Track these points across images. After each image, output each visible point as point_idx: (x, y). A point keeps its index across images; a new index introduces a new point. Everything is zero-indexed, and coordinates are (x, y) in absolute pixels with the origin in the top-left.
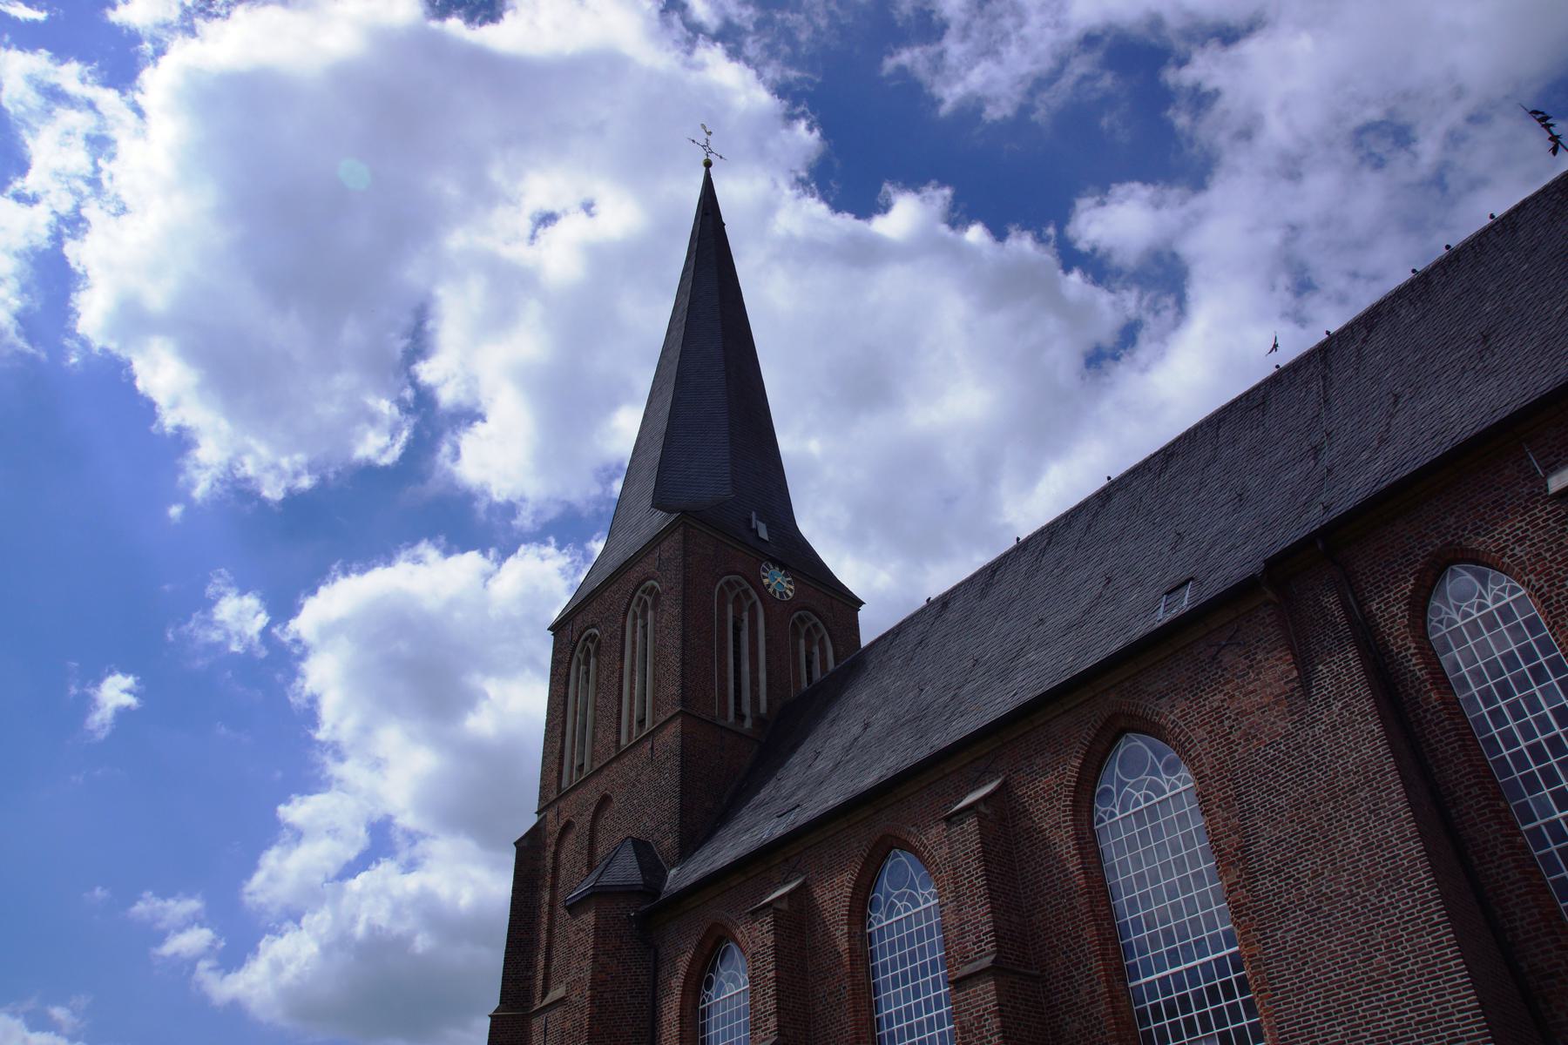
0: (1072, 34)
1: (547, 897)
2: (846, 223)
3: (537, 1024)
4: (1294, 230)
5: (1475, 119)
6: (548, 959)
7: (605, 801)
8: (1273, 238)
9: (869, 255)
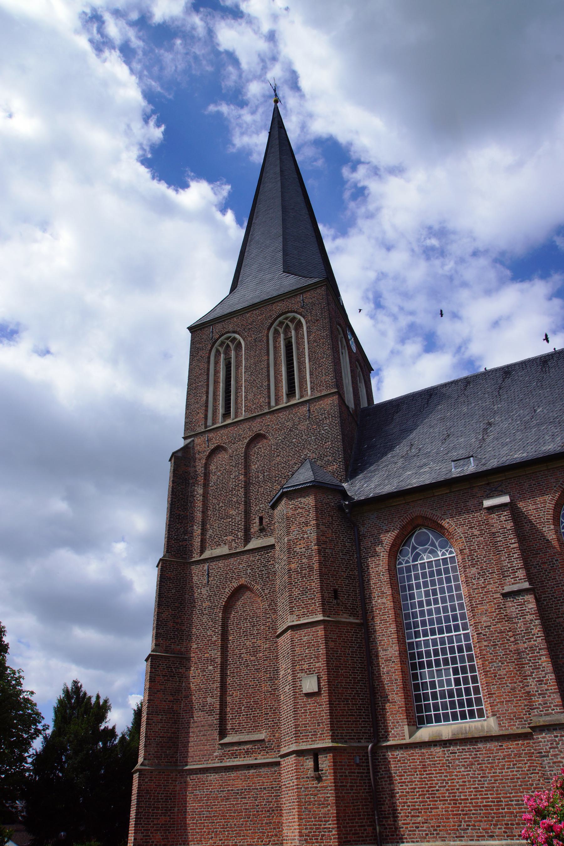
0: (310, 137)
1: (201, 491)
2: (162, 187)
3: (195, 569)
4: (382, 276)
5: (475, 254)
6: (204, 531)
7: (258, 437)
8: (372, 275)
9: (167, 209)
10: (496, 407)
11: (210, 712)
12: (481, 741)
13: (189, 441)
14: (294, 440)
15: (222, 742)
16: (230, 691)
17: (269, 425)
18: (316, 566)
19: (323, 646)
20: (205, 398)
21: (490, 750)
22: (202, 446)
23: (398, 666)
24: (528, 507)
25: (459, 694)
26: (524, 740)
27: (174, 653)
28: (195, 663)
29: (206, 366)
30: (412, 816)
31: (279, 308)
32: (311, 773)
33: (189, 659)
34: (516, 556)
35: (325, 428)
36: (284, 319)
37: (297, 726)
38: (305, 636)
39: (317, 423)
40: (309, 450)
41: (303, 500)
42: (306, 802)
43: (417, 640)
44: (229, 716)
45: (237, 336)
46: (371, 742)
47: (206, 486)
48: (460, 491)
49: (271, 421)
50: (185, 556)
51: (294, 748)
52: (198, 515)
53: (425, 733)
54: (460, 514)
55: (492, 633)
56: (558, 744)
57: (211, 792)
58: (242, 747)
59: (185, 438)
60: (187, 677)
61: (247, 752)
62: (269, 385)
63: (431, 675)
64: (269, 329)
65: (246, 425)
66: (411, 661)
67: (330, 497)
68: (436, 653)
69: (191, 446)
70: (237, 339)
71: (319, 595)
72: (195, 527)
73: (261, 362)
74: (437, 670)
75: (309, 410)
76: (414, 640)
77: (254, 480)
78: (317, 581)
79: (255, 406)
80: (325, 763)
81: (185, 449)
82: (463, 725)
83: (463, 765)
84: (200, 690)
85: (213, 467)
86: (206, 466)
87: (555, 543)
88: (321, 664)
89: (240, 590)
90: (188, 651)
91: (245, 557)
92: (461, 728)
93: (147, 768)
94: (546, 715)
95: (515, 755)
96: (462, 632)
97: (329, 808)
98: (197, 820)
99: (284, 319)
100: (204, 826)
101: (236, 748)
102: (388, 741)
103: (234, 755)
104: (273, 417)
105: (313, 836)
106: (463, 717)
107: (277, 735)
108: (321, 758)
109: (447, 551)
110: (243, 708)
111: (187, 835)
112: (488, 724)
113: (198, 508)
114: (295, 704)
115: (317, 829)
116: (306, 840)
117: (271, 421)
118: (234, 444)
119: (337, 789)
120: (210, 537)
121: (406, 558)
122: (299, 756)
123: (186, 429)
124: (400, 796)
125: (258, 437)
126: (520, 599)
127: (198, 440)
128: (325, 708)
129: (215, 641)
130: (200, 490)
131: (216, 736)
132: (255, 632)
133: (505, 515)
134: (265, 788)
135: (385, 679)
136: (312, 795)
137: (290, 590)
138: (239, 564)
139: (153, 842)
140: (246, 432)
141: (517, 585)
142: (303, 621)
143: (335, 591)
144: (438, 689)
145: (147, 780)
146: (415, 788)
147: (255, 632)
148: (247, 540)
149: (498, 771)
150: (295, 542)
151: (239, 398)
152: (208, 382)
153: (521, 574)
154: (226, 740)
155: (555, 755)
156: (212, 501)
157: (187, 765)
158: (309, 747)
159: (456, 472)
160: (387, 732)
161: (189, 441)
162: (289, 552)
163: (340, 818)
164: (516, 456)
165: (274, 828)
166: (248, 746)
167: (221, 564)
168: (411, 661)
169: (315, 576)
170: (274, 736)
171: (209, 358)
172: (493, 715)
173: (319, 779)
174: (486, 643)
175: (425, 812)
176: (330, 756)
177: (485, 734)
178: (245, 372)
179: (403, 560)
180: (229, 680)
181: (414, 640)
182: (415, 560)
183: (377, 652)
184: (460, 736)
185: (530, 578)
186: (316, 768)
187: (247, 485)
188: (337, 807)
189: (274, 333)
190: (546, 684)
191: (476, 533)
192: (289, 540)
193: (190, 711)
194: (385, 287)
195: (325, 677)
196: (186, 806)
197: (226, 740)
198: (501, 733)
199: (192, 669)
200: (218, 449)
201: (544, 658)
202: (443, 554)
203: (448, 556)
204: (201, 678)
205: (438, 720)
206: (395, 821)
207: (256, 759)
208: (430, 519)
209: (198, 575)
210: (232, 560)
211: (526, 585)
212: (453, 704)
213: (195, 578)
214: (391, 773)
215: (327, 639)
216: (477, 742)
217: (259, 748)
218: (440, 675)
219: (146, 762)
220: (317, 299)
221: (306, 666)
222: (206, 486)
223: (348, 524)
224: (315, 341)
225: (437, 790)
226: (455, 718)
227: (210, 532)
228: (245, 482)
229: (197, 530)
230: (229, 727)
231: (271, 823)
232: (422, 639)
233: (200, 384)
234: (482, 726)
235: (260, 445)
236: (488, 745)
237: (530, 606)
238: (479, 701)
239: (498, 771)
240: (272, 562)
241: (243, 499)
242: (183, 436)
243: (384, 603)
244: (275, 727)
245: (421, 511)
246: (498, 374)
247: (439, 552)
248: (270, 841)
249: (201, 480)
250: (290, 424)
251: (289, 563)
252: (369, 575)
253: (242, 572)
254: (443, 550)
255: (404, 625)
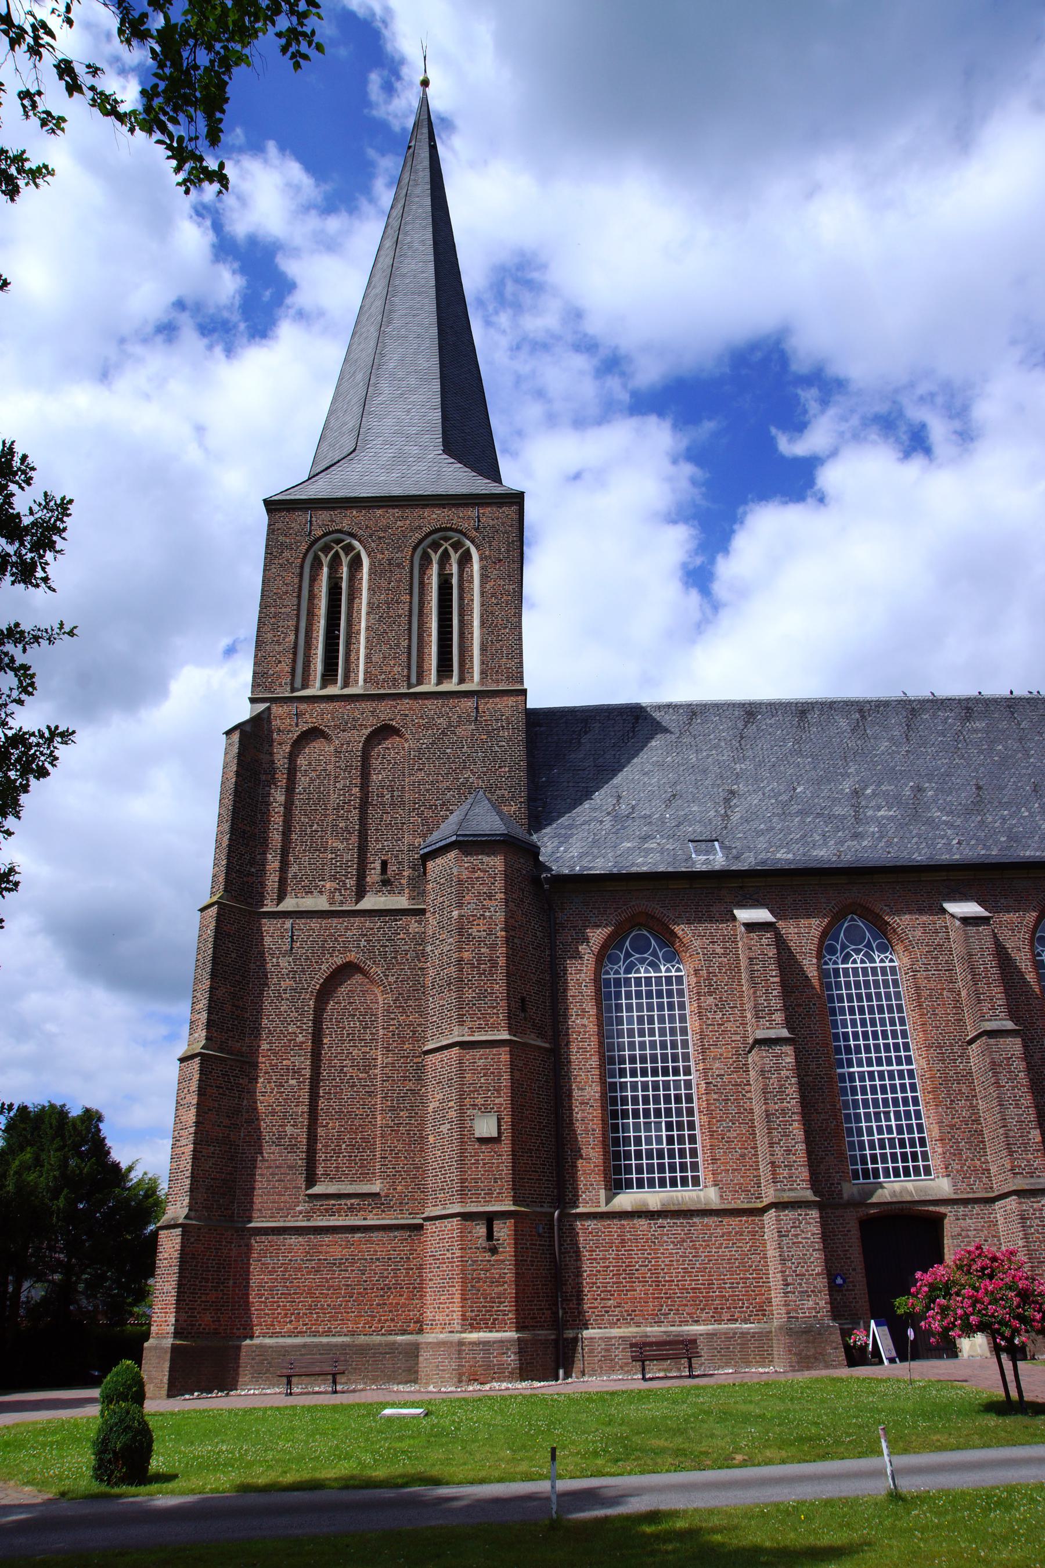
6: (284, 865)
7: (385, 731)
10: (738, 766)
11: (292, 1148)
12: (698, 1215)
13: (262, 707)
14: (448, 751)
15: (310, 1192)
16: (323, 1119)
17: (407, 715)
18: (502, 961)
19: (506, 1076)
20: (292, 637)
21: (707, 1225)
22: (286, 724)
23: (598, 1113)
24: (789, 929)
25: (672, 1155)
26: (749, 1216)
27: (231, 1054)
28: (266, 1073)
29: (296, 580)
30: (602, 1299)
31: (434, 516)
32: (482, 1242)
33: (255, 1065)
34: (775, 993)
35: (501, 744)
36: (441, 539)
37: (463, 1181)
38: (480, 1059)
39: (488, 733)
40: (474, 773)
41: (486, 859)
42: (473, 1279)
43: (623, 1080)
44: (321, 1156)
45: (356, 543)
46: (558, 1208)
47: (290, 790)
48: (710, 893)
49: (411, 709)
50: (251, 901)
51: (457, 1209)
52: (276, 838)
53: (625, 1200)
54: (700, 922)
55: (724, 1085)
56: (801, 1223)
57: (291, 1260)
58: (343, 1202)
59: (253, 700)
60: (252, 1093)
61: (351, 1209)
62: (409, 647)
63: (637, 1128)
64: (415, 549)
65: (368, 706)
66: (613, 1108)
67: (522, 860)
68: (646, 1100)
69: (265, 716)
70: (354, 549)
71: (504, 1003)
72: (269, 857)
73: (398, 603)
74: (645, 1123)
75: (477, 708)
76: (617, 1080)
77: (374, 799)
78: (503, 983)
79: (383, 676)
80: (503, 1231)
81: (256, 721)
82: (674, 1194)
83: (673, 1242)
84: (273, 1113)
85: (302, 761)
86: (292, 757)
87: (815, 982)
88: (503, 1100)
89: (347, 970)
90: (254, 1051)
91: (357, 921)
92: (672, 1197)
93: (194, 1222)
94: (790, 1190)
95: (736, 1233)
96: (682, 1077)
97: (506, 1286)
98: (267, 1298)
99: (441, 539)
100: (279, 1306)
101: (333, 1202)
102: (578, 1207)
103: (330, 1212)
104: (416, 704)
105: (481, 1320)
106: (673, 1184)
107: (399, 1188)
108: (497, 1225)
109: (673, 966)
110: (344, 1146)
111: (250, 1317)
112: (708, 1195)
113: (276, 826)
114: (462, 1152)
115: (487, 1311)
116: (470, 1324)
117: (411, 709)
118: (344, 731)
119: (518, 1263)
120: (295, 876)
121: (616, 967)
122: (466, 1220)
123: (255, 685)
124: (588, 1275)
125: (385, 731)
126: (777, 1049)
127: (277, 710)
128: (506, 1159)
129: (303, 1043)
130: (279, 797)
131: (301, 1182)
132: (368, 1037)
133: (768, 937)
134: (378, 1259)
135: (579, 1127)
136: (482, 1270)
137: (460, 990)
138: (347, 929)
139: (200, 1325)
140: (370, 716)
141: (773, 1031)
142: (477, 1037)
143: (523, 999)
144: (644, 1147)
145: (192, 1240)
146: (609, 1267)
147: (368, 1037)
148: (360, 894)
149: (714, 1250)
150: (472, 919)
151: (353, 654)
152: (298, 610)
153: (779, 1017)
154: (317, 1190)
155: (796, 1236)
156: (299, 818)
157: (250, 1222)
158: (481, 1209)
159: (700, 862)
160: (576, 1196)
161: (262, 707)
162: (460, 934)
163: (518, 1299)
164: (778, 856)
165: (390, 1311)
166: (353, 1201)
167: (314, 924)
168: (613, 1108)
169: (500, 975)
170: (395, 1189)
171: (302, 567)
172: (716, 1185)
173: (494, 1251)
174: (715, 1096)
175: (619, 1295)
176: (510, 1222)
177: (703, 1207)
178: (368, 613)
179: (612, 969)
180: (322, 1104)
181: (617, 1080)
182: (628, 971)
183: (570, 1090)
184: (673, 1208)
185: (789, 1024)
186: (490, 1236)
187: (364, 804)
188: (516, 1285)
189: (422, 558)
190: (794, 1154)
191: (719, 950)
192: (461, 916)
193: (256, 1142)
194: (200, 209)
195: (507, 1119)
196: (249, 1279)
197: (317, 1190)
198: (723, 1207)
199: (261, 1080)
200: (314, 734)
201: (796, 1124)
202: (668, 970)
203: (673, 974)
204: (276, 1095)
205: (640, 1184)
206: (579, 1304)
207: (365, 1219)
208: (658, 920)
209: (273, 935)
210: (335, 921)
211: (785, 1033)
212: (661, 1168)
213: (267, 940)
214: (579, 1248)
215: (513, 1067)
216: (692, 1215)
217: (369, 1205)
218: (648, 1129)
219: (193, 1214)
220: (503, 524)
221: (480, 1101)
222: (290, 790)
223: (548, 909)
224: (493, 595)
225: (637, 1270)
226: (662, 1183)
227: (293, 869)
228: (361, 799)
229: (273, 863)
230: (320, 1171)
231: (385, 1304)
232: (629, 1079)
233: (283, 610)
234: (698, 1197)
235: (387, 743)
236: (706, 1220)
237: (788, 1060)
238: (695, 1167)
239: (714, 1250)
240: (402, 936)
241: (357, 827)
242: (250, 695)
243: (584, 1025)
244: (417, 1175)
245: (652, 906)
246: (737, 713)
247: (662, 967)
248: (382, 1327)
249: (282, 778)
250: (442, 722)
251: (460, 950)
252: (566, 982)
253: (350, 942)
254: (668, 965)
255: (609, 1061)
